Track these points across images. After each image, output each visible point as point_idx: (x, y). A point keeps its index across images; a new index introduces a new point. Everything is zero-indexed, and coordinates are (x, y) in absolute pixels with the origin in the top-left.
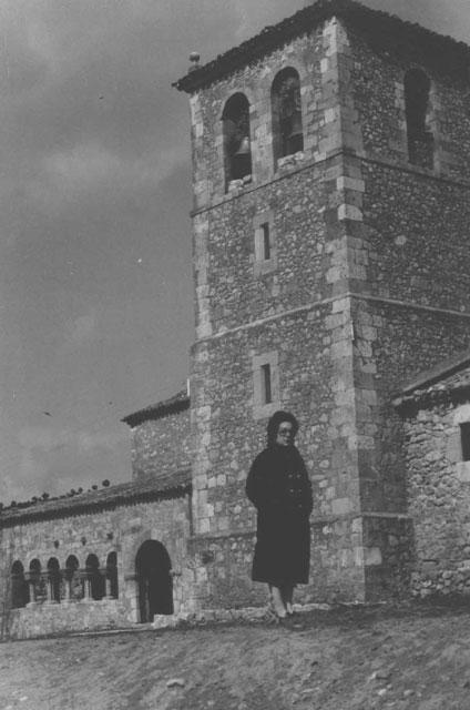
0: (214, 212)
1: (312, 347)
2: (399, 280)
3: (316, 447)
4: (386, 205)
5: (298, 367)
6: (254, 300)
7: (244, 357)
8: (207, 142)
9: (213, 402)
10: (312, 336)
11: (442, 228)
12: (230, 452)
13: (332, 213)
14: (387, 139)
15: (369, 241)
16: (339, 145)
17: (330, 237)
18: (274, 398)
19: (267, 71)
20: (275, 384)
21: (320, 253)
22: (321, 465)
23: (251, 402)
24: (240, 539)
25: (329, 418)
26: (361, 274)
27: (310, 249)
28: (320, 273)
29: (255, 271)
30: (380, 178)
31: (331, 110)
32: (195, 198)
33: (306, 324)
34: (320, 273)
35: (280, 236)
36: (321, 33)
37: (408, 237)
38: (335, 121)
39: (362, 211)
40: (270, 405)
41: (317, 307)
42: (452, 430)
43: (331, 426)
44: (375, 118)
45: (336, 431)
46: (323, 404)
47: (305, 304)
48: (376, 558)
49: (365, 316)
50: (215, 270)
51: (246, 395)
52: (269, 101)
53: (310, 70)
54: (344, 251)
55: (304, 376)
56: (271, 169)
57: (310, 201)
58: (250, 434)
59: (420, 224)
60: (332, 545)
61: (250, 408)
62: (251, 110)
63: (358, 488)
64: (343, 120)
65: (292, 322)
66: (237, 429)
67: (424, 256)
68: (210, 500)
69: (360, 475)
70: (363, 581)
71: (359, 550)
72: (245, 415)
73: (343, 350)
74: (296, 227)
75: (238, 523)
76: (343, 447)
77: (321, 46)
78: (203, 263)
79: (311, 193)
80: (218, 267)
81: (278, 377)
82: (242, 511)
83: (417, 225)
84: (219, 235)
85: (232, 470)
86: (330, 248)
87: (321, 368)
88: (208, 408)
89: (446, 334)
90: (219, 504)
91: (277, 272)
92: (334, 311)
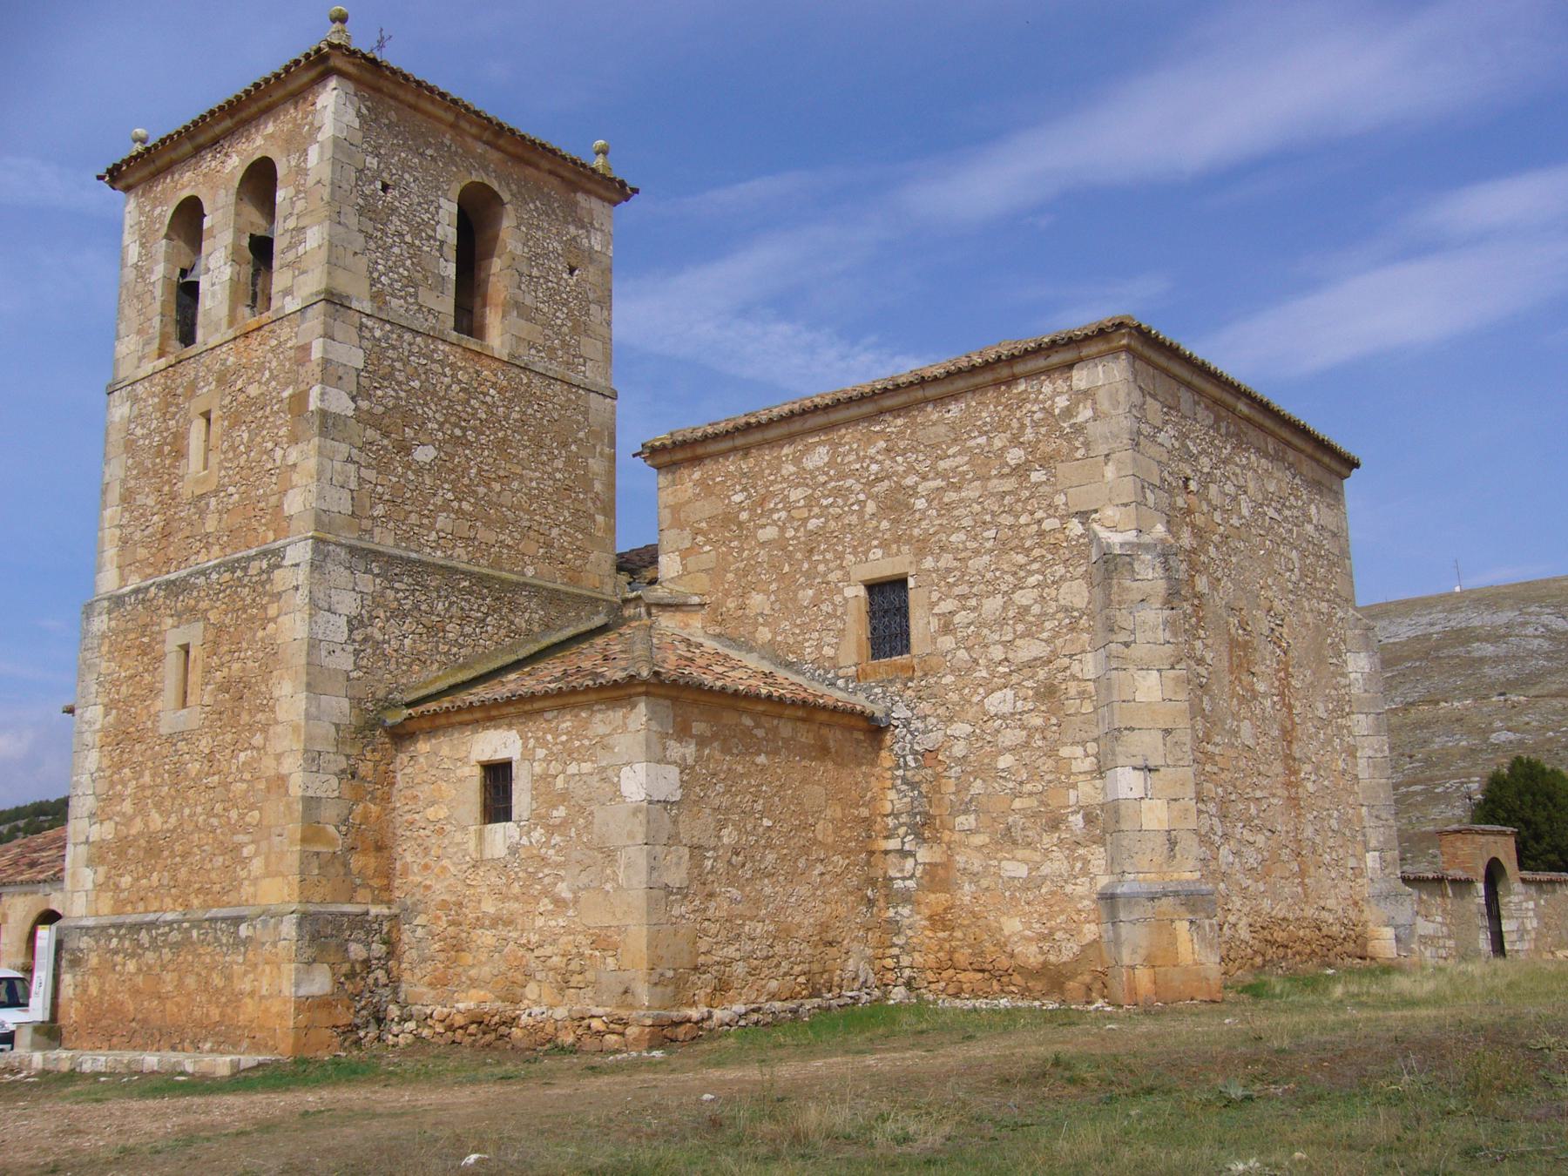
0: (139, 388)
1: (252, 619)
2: (414, 518)
3: (245, 786)
4: (403, 394)
5: (231, 652)
6: (180, 535)
7: (156, 628)
8: (142, 273)
9: (106, 700)
10: (254, 600)
11: (504, 440)
12: (124, 784)
13: (300, 399)
14: (416, 286)
15: (360, 449)
16: (323, 286)
17: (294, 439)
18: (191, 699)
19: (234, 162)
20: (195, 677)
21: (278, 463)
22: (248, 819)
23: (159, 705)
24: (123, 931)
25: (266, 739)
26: (341, 503)
27: (265, 457)
28: (276, 497)
29: (186, 490)
30: (394, 348)
31: (316, 228)
32: (115, 364)
33: (246, 580)
34: (276, 497)
35: (227, 433)
36: (314, 104)
37: (439, 449)
38: (320, 247)
39: (353, 399)
40: (185, 711)
41: (264, 554)
42: (466, 771)
43: (266, 754)
44: (396, 250)
45: (273, 763)
46: (260, 716)
47: (250, 548)
48: (320, 982)
49: (340, 575)
50: (132, 483)
51: (153, 691)
52: (232, 209)
53: (293, 163)
54: (312, 463)
55: (236, 666)
56: (225, 322)
57: (273, 377)
58: (154, 758)
59: (464, 429)
60: (250, 955)
61: (157, 714)
62: (207, 223)
63: (297, 863)
64: (331, 244)
65: (227, 576)
66: (137, 747)
67: (466, 481)
68: (91, 862)
69: (304, 840)
70: (291, 1024)
71: (289, 969)
72: (149, 724)
73: (292, 627)
74: (250, 418)
75: (124, 906)
76: (282, 790)
77: (312, 124)
78: (115, 470)
79: (274, 364)
80: (136, 478)
81: (200, 663)
82: (132, 886)
83: (458, 432)
84: (143, 426)
85: (124, 814)
86: (294, 455)
87: (261, 655)
88: (100, 709)
89: (493, 610)
90: (102, 870)
91: (216, 493)
92: (286, 562)
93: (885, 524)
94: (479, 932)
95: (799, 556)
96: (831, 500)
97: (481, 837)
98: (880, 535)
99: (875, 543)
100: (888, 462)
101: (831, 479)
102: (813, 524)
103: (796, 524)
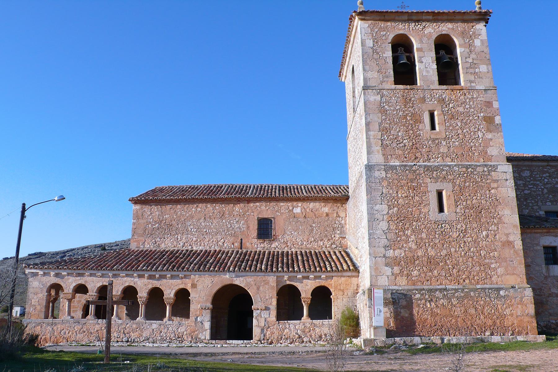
93: (551, 196)
94: (551, 298)
95: (522, 200)
96: (532, 186)
97: (548, 270)
98: (549, 199)
99: (548, 200)
100: (550, 180)
101: (531, 180)
102: (526, 192)
103: (520, 191)
